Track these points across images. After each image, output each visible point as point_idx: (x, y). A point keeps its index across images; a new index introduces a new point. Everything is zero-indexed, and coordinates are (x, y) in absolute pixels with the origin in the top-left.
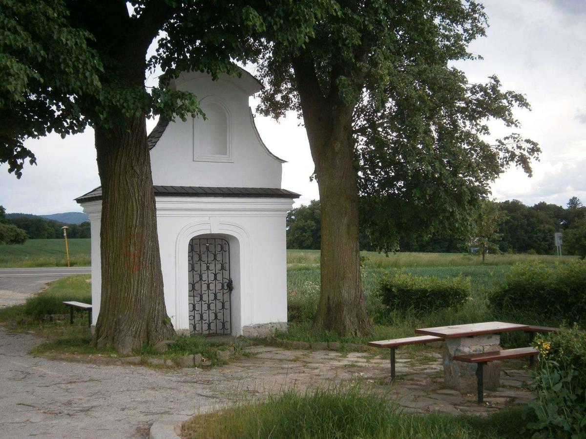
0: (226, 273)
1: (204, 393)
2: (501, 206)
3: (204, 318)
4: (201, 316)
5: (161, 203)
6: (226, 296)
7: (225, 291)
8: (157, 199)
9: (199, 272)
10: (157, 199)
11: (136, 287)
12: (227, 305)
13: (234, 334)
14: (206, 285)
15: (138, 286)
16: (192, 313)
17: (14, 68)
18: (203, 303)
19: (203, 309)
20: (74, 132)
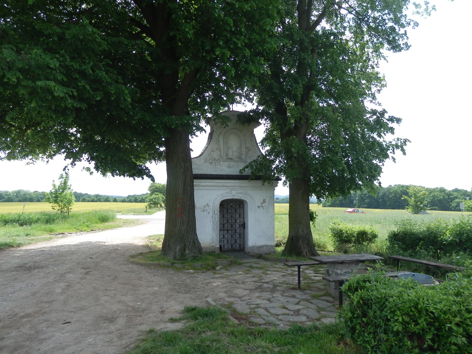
0: (242, 220)
1: (177, 255)
2: (344, 192)
3: (229, 242)
4: (228, 241)
5: (196, 182)
6: (242, 231)
7: (241, 228)
8: (195, 181)
9: (227, 218)
10: (195, 181)
11: (179, 225)
12: (242, 236)
13: (246, 250)
14: (230, 225)
15: (180, 225)
16: (222, 232)
17: (264, 310)
18: (229, 224)
19: (228, 217)
20: (149, 172)
